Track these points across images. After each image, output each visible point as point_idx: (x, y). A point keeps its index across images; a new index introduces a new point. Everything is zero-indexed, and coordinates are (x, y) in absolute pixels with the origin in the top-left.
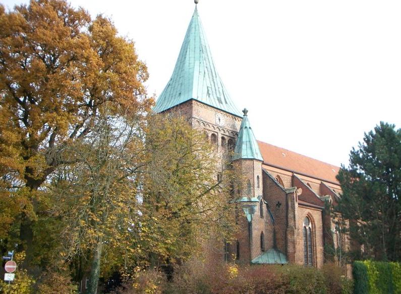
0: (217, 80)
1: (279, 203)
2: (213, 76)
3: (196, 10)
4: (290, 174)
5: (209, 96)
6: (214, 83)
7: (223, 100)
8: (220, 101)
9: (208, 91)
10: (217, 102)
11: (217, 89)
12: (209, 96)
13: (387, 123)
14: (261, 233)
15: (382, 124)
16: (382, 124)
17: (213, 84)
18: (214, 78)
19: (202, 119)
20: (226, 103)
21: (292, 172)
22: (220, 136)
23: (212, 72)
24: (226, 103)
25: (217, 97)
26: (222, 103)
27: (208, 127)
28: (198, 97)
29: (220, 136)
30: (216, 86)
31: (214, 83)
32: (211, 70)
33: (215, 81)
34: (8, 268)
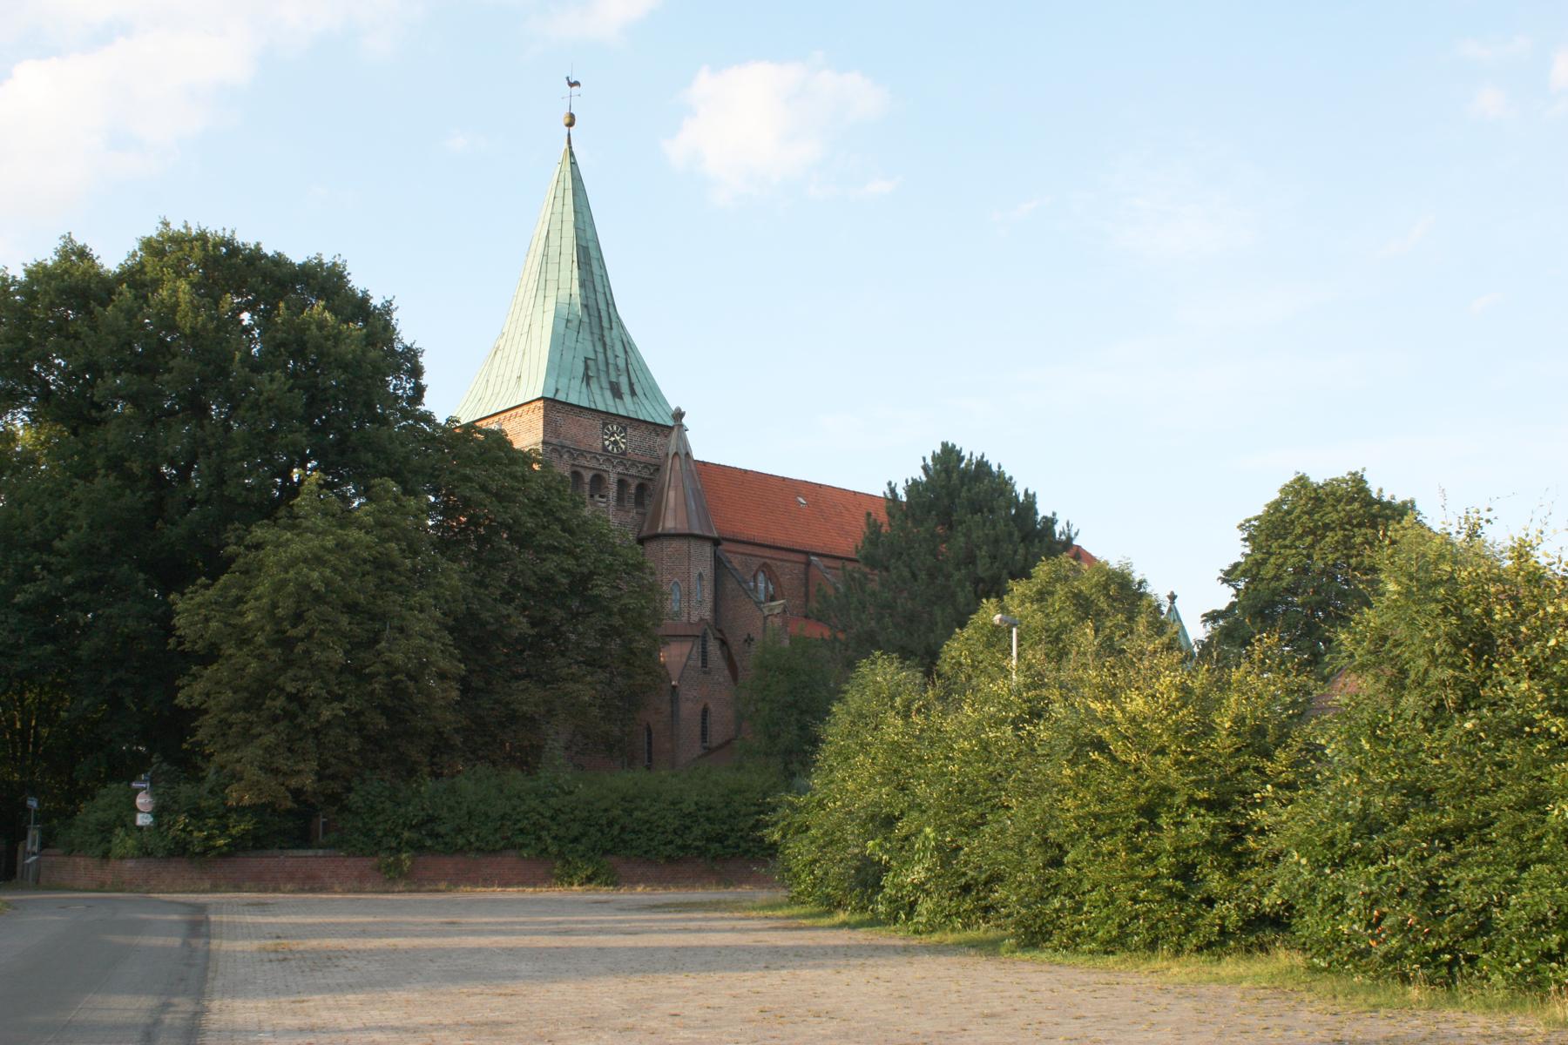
0: (612, 337)
1: (749, 635)
2: (602, 328)
3: (569, 135)
4: (802, 558)
6: (604, 345)
7: (625, 389)
9: (587, 368)
10: (608, 394)
11: (611, 361)
13: (1229, 577)
14: (701, 707)
15: (944, 445)
16: (944, 445)
17: (600, 349)
18: (606, 333)
19: (568, 443)
20: (633, 393)
21: (807, 553)
22: (612, 479)
23: (600, 317)
24: (633, 393)
25: (611, 383)
27: (583, 462)
28: (557, 390)
29: (612, 479)
30: (609, 353)
31: (604, 345)
33: (608, 340)
34: (142, 804)
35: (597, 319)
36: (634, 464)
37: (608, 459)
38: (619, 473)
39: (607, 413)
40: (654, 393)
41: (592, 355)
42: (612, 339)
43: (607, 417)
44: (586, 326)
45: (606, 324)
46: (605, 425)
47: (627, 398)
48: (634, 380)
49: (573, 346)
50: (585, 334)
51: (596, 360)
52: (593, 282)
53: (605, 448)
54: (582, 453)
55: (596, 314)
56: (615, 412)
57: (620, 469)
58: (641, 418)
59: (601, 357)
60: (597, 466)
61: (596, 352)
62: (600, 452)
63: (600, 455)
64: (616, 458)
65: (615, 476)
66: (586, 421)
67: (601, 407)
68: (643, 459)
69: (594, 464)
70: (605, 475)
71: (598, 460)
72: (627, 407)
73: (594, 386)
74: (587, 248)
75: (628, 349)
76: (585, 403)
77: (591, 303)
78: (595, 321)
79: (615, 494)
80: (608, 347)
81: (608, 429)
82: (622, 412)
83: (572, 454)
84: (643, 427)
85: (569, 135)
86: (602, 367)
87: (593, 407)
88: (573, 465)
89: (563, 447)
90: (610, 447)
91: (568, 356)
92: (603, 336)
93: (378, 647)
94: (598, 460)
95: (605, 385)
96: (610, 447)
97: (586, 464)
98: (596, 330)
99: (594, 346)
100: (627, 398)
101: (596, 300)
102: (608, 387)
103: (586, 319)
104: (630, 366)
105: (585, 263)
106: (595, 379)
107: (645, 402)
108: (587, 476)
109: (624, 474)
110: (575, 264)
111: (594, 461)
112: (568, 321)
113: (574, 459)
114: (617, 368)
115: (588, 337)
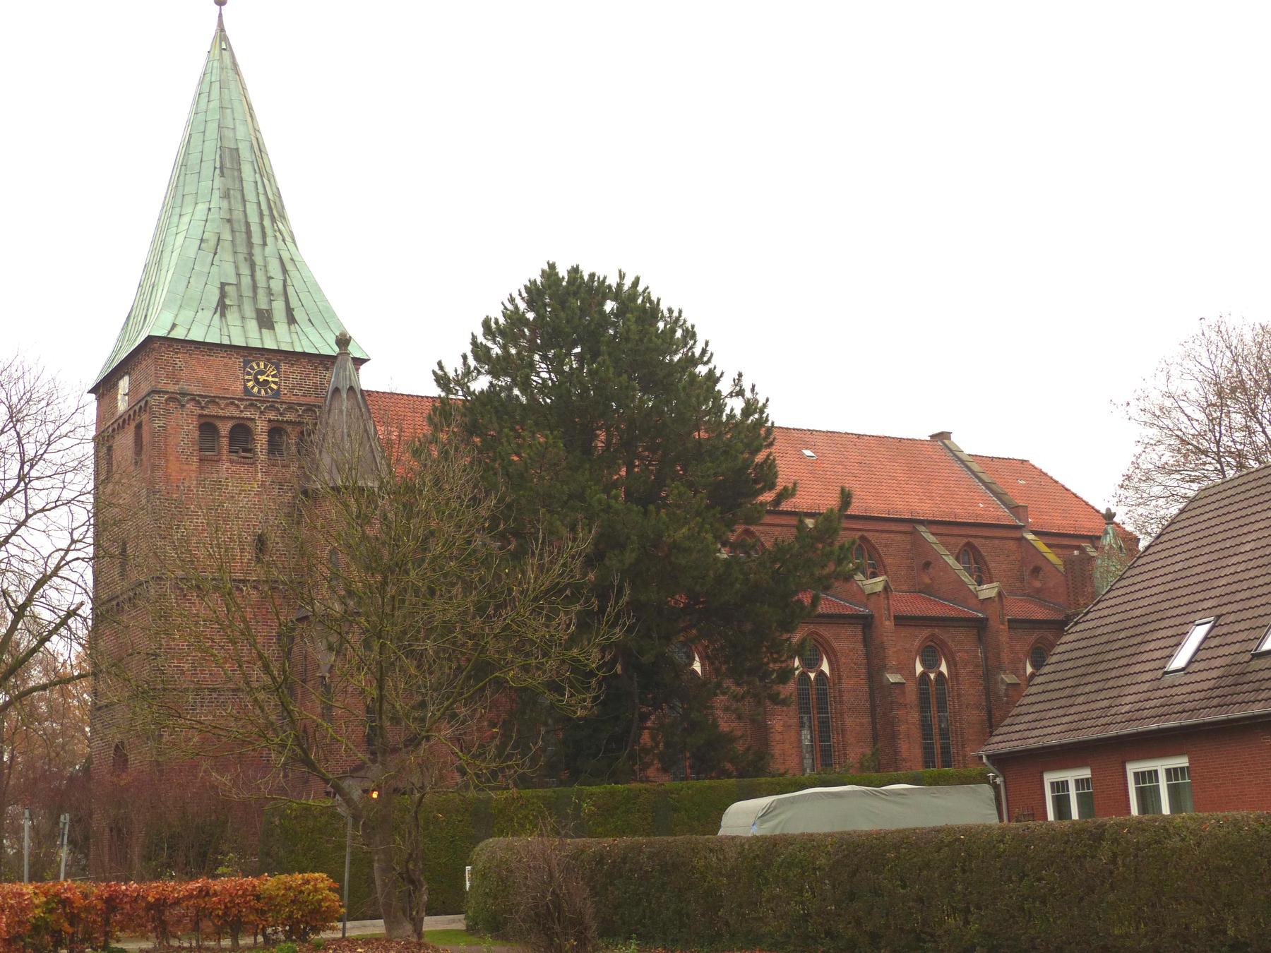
0: (267, 257)
2: (250, 245)
3: (220, 16)
4: (794, 521)
5: (223, 315)
6: (252, 266)
8: (265, 321)
9: (223, 295)
10: (253, 325)
11: (261, 282)
12: (223, 315)
17: (245, 270)
18: (257, 251)
19: (195, 390)
20: (291, 320)
22: (261, 428)
23: (249, 233)
24: (291, 320)
26: (273, 328)
27: (213, 410)
28: (174, 326)
29: (261, 428)
30: (260, 275)
31: (252, 266)
32: (248, 224)
33: (258, 259)
35: (244, 236)
36: (291, 407)
37: (251, 405)
38: (270, 421)
39: (247, 348)
40: (325, 316)
41: (233, 280)
42: (265, 258)
43: (249, 353)
44: (228, 245)
45: (257, 239)
46: (246, 363)
47: (281, 327)
48: (294, 302)
49: (206, 270)
50: (225, 255)
51: (238, 285)
52: (242, 190)
53: (247, 391)
54: (213, 401)
55: (243, 229)
56: (228, 343)
57: (271, 415)
58: (299, 349)
59: (246, 281)
60: (236, 413)
61: (238, 275)
62: (241, 395)
63: (240, 400)
64: (264, 402)
65: (265, 424)
66: (218, 360)
67: (238, 341)
68: (303, 400)
69: (231, 412)
70: (250, 424)
71: (238, 406)
72: (282, 338)
73: (233, 317)
74: (237, 149)
75: (289, 267)
76: (213, 338)
77: (238, 215)
78: (241, 237)
79: (266, 446)
80: (257, 268)
81: (252, 368)
82: (270, 344)
83: (199, 402)
84: (304, 361)
85: (220, 16)
86: (247, 292)
87: (226, 342)
88: (201, 416)
89: (184, 394)
90: (256, 390)
91: (196, 284)
92: (251, 254)
93: (45, 899)
94: (238, 406)
95: (249, 311)
96: (256, 390)
97: (221, 413)
98: (242, 249)
99: (237, 268)
100: (281, 327)
101: (245, 212)
102: (254, 315)
103: (227, 236)
104: (290, 290)
105: (232, 169)
106: (235, 309)
107: (309, 330)
108: (225, 428)
109: (278, 421)
110: (218, 171)
111: (232, 408)
112: (202, 240)
113: (202, 408)
114: (270, 292)
115: (229, 257)
